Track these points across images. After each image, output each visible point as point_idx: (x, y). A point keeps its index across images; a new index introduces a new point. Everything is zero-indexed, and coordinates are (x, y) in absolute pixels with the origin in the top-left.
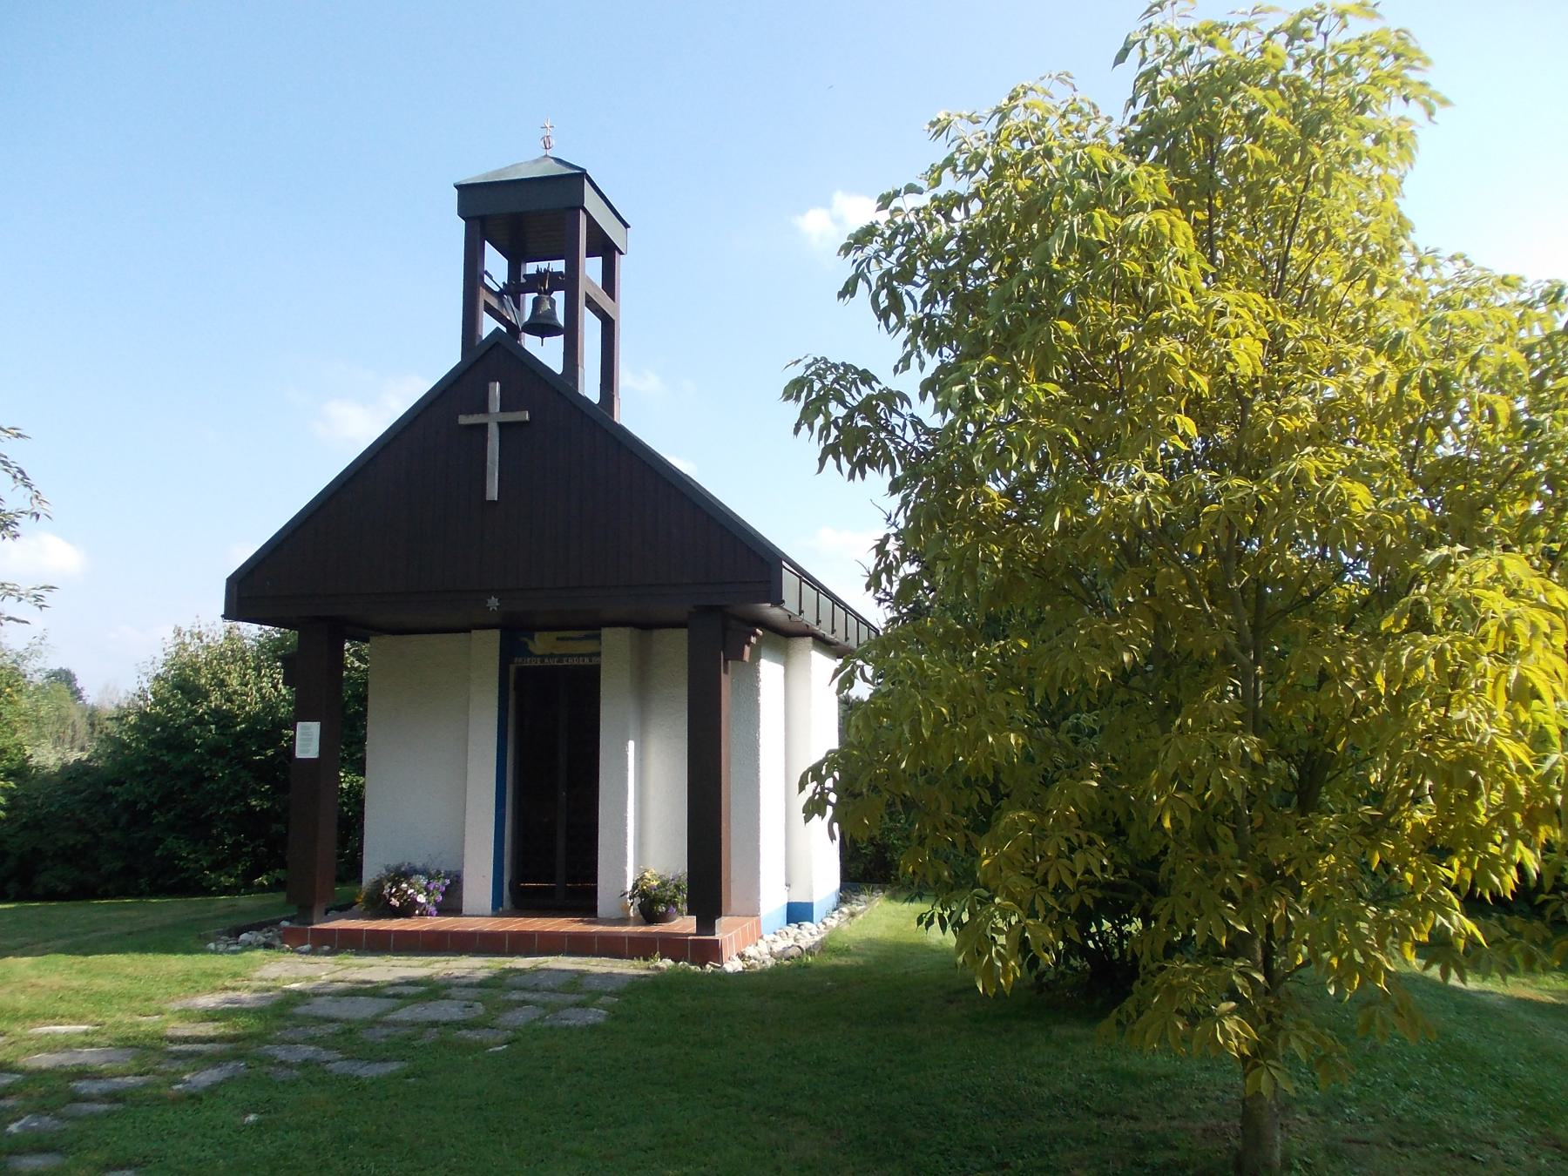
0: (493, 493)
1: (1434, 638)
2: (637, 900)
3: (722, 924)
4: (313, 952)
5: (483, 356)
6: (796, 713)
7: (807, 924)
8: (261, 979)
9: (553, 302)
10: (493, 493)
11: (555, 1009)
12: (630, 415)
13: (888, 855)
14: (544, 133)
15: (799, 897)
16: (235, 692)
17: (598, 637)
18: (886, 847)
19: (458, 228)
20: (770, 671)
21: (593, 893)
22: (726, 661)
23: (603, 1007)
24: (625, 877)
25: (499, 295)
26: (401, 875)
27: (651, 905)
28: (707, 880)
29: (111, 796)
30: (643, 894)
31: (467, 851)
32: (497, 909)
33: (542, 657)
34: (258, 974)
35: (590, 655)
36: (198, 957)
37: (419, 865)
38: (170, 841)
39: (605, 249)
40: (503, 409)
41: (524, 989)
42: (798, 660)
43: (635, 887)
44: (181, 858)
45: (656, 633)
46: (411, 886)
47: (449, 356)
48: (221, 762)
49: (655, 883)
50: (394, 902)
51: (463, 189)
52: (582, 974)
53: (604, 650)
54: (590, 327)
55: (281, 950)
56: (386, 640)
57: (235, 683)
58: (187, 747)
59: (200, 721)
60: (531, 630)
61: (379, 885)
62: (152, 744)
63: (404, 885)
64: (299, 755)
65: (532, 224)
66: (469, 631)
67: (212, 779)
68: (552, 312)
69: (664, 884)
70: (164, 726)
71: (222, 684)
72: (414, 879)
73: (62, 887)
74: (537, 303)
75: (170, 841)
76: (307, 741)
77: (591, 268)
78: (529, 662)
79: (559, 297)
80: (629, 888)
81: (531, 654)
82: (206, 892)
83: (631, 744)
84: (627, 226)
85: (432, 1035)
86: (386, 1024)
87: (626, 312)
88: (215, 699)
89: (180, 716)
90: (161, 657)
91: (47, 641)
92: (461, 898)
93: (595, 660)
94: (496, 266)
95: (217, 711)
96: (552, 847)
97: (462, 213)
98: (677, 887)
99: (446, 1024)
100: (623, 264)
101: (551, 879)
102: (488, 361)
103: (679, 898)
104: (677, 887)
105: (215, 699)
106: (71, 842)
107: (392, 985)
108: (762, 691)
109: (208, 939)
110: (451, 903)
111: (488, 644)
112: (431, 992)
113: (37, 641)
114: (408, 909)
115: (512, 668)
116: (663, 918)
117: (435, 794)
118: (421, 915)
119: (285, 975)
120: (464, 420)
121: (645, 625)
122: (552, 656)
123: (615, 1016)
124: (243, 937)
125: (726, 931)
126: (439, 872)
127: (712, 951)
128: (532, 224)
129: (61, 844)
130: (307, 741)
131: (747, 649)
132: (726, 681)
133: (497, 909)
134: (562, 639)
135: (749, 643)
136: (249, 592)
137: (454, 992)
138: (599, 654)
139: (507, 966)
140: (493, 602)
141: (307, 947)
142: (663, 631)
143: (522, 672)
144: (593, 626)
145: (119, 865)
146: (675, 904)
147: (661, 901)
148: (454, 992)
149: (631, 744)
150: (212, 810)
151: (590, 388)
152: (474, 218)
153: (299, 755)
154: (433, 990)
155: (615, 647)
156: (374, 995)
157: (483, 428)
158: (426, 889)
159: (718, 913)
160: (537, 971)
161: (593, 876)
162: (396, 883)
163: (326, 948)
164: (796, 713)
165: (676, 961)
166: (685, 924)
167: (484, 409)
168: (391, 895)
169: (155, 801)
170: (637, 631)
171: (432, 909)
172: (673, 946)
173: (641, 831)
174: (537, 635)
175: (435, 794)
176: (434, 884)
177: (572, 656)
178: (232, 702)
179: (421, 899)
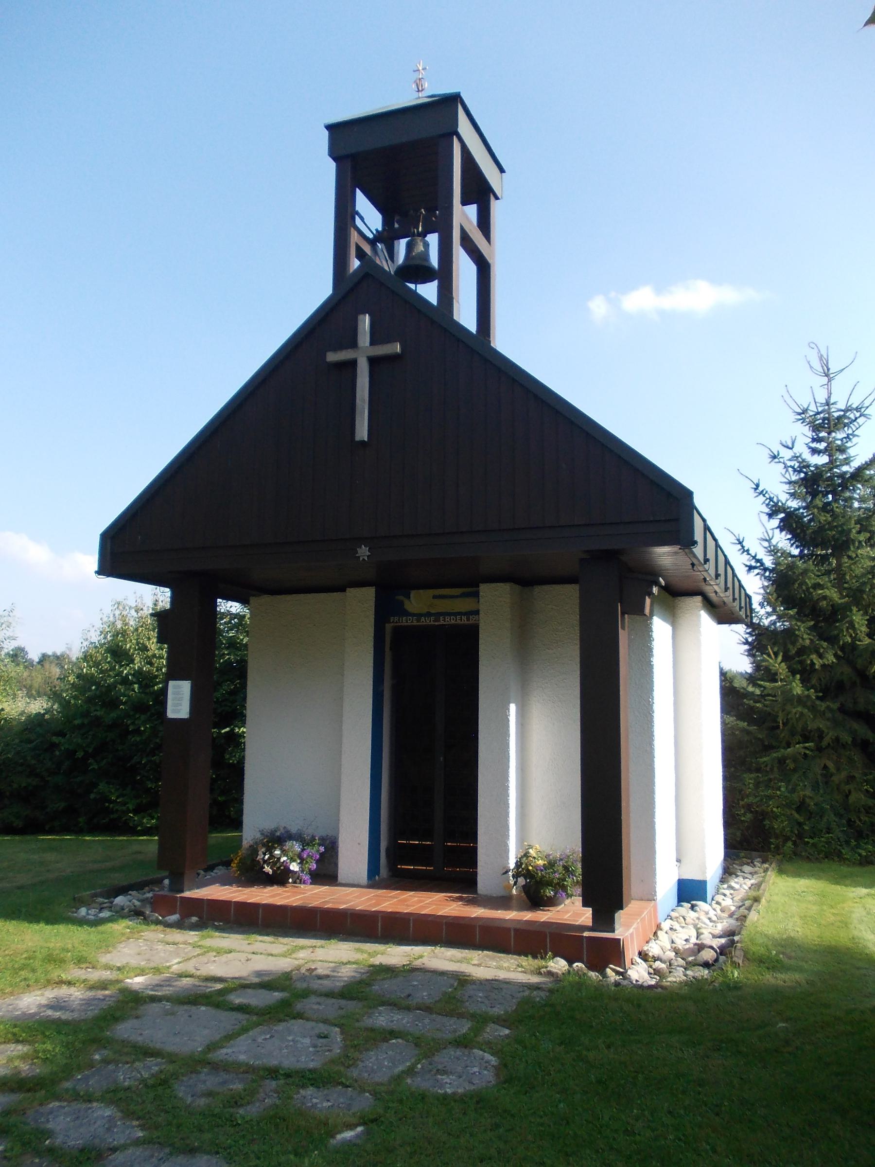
0: (362, 432)
1: (815, 661)
2: (521, 881)
3: (620, 917)
4: (179, 925)
5: (352, 290)
6: (690, 673)
7: (700, 903)
8: (107, 967)
9: (426, 245)
10: (362, 432)
11: (426, 1047)
12: (507, 342)
13: (767, 822)
14: (416, 76)
15: (691, 874)
16: (154, 656)
17: (476, 595)
18: (764, 815)
19: (327, 171)
20: (660, 629)
21: (470, 857)
22: (623, 614)
23: (489, 1046)
24: (507, 851)
25: (372, 242)
26: (275, 840)
27: (536, 888)
28: (604, 864)
29: (54, 746)
30: (528, 875)
31: (341, 818)
32: (374, 880)
33: (419, 616)
34: (104, 959)
35: (468, 614)
36: (61, 928)
37: (294, 830)
38: (102, 787)
39: (479, 192)
40: (373, 342)
41: (394, 1005)
42: (686, 620)
43: (518, 864)
44: (110, 802)
45: (538, 590)
46: (284, 852)
47: (318, 288)
48: (143, 717)
49: (541, 862)
50: (268, 869)
51: (333, 129)
52: (462, 980)
53: (482, 607)
54: (465, 271)
55: (146, 920)
56: (266, 599)
57: (153, 647)
58: (113, 704)
59: (125, 681)
60: (407, 588)
61: (253, 850)
62: (89, 700)
63: (277, 852)
64: (171, 714)
65: (407, 166)
66: (342, 589)
67: (137, 731)
68: (425, 255)
69: (551, 864)
70: (98, 684)
71: (145, 649)
72: (288, 844)
73: (18, 823)
74: (410, 247)
75: (102, 787)
76: (179, 701)
77: (465, 215)
78: (405, 621)
79: (433, 239)
80: (512, 865)
81: (407, 614)
82: (132, 831)
83: (513, 707)
84: (502, 170)
85: (268, 1097)
86: (216, 1067)
87: (501, 252)
88: (138, 663)
89: (109, 676)
90: (99, 625)
91: (15, 613)
92: (336, 865)
93: (472, 620)
94: (370, 217)
95: (139, 673)
96: (430, 814)
97: (335, 154)
98: (566, 868)
99: (288, 1076)
100: (497, 208)
101: (427, 834)
102: (360, 289)
103: (569, 881)
104: (566, 868)
105: (138, 663)
106: (24, 785)
107: (244, 986)
108: (655, 652)
109: (79, 902)
110: (326, 873)
111: (362, 602)
112: (285, 1004)
113: (6, 613)
114: (281, 877)
115: (388, 627)
116: (551, 902)
117: (313, 756)
118: (295, 882)
119: (134, 962)
120: (333, 357)
121: (526, 579)
122: (429, 614)
123: (507, 1076)
124: (120, 900)
125: (627, 928)
126: (313, 838)
127: (609, 953)
128: (407, 166)
129: (15, 786)
130: (179, 701)
131: (648, 601)
132: (623, 635)
133: (374, 880)
134: (435, 597)
135: (650, 594)
136: (125, 550)
137: (311, 1005)
138: (477, 613)
139: (378, 960)
140: (363, 552)
141: (175, 917)
142: (546, 588)
143: (397, 630)
144: (470, 583)
145: (62, 805)
146: (564, 888)
147: (549, 883)
148: (311, 1005)
149: (513, 707)
150: (136, 759)
151: (466, 315)
152: (346, 157)
153: (171, 714)
154: (285, 998)
155: (495, 603)
156: (217, 1006)
157: (352, 364)
158: (300, 856)
159: (619, 905)
160: (410, 971)
161: (472, 835)
162: (270, 850)
163: (194, 919)
164: (690, 673)
165: (570, 962)
166: (573, 911)
167: (352, 343)
168: (265, 862)
169: (90, 750)
170: (517, 588)
171: (306, 877)
172: (563, 941)
173: (527, 800)
174: (413, 594)
175: (313, 756)
176: (310, 850)
177: (449, 614)
178: (151, 664)
179: (294, 867)
